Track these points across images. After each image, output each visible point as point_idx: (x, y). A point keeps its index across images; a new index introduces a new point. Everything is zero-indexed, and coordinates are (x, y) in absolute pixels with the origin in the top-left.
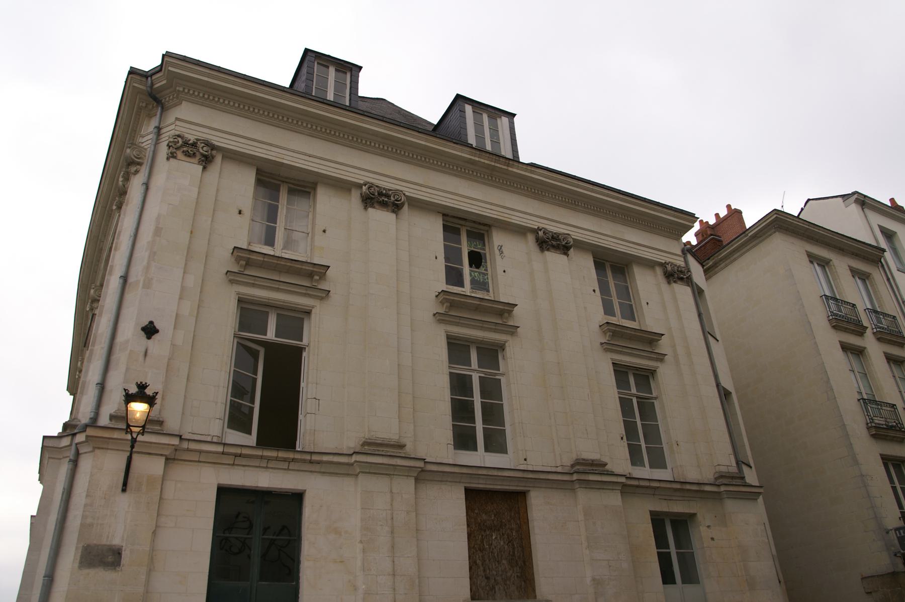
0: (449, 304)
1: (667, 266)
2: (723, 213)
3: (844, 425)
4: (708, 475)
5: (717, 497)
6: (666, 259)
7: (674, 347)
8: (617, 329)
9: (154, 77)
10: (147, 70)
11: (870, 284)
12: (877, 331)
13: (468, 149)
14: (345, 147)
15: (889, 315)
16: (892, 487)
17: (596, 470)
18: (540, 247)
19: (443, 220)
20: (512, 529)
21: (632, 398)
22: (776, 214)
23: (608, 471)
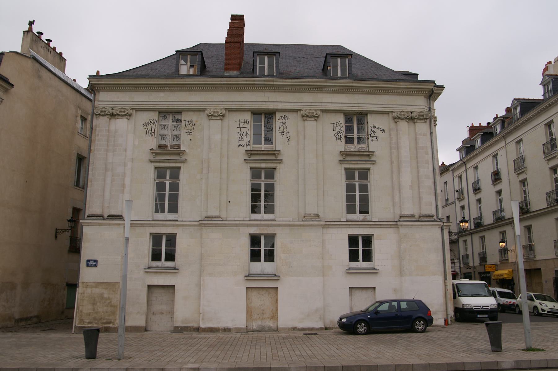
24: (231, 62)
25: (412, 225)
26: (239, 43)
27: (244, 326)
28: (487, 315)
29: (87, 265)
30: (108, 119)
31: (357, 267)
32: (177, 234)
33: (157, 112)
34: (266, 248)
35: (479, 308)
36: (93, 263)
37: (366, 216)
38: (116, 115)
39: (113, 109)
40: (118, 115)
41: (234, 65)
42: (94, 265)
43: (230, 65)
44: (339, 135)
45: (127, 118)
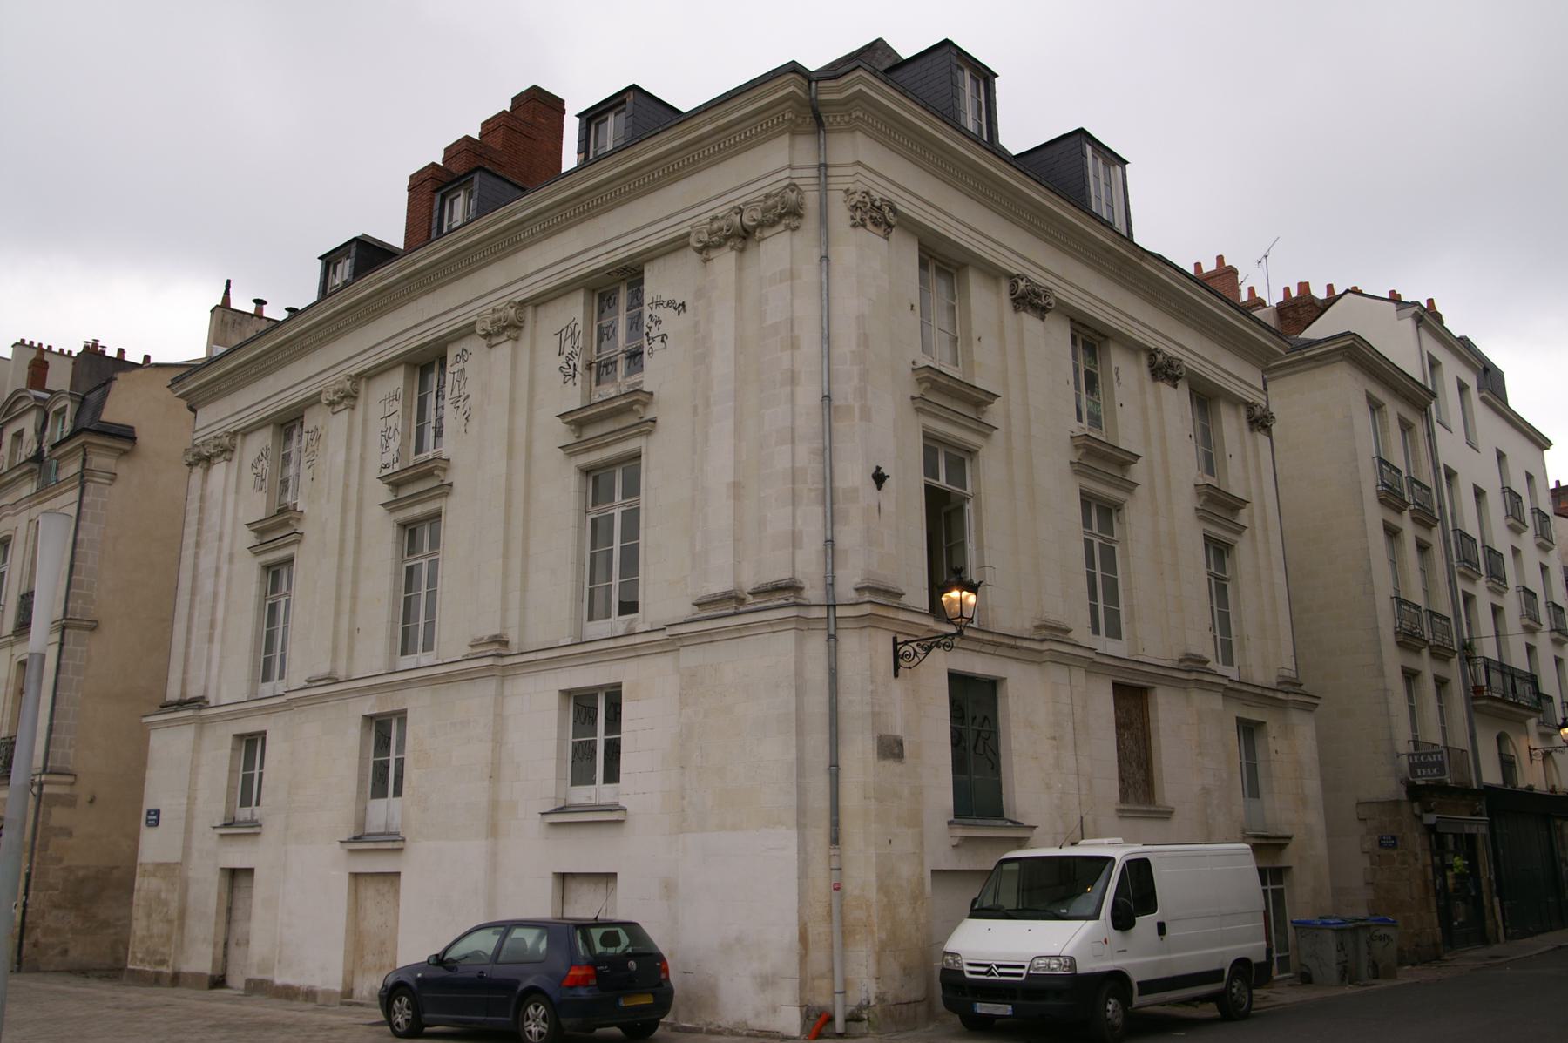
0: (1085, 451)
1: (1020, 281)
2: (1209, 266)
3: (1378, 627)
4: (1272, 681)
5: (1282, 705)
6: (1255, 398)
7: (1008, 417)
8: (950, 384)
9: (821, 84)
10: (811, 70)
11: (1379, 417)
12: (1415, 509)
13: (1111, 233)
14: (945, 184)
15: (1395, 468)
16: (1410, 706)
17: (1057, 636)
18: (1153, 375)
19: (1072, 328)
20: (1137, 729)
21: (1094, 539)
22: (1353, 339)
23: (1209, 669)
25: (708, 632)
27: (339, 988)
28: (1010, 1007)
31: (588, 802)
34: (577, 738)
35: (985, 969)
37: (632, 621)
38: (755, 228)
39: (740, 211)
44: (571, 363)
45: (787, 227)
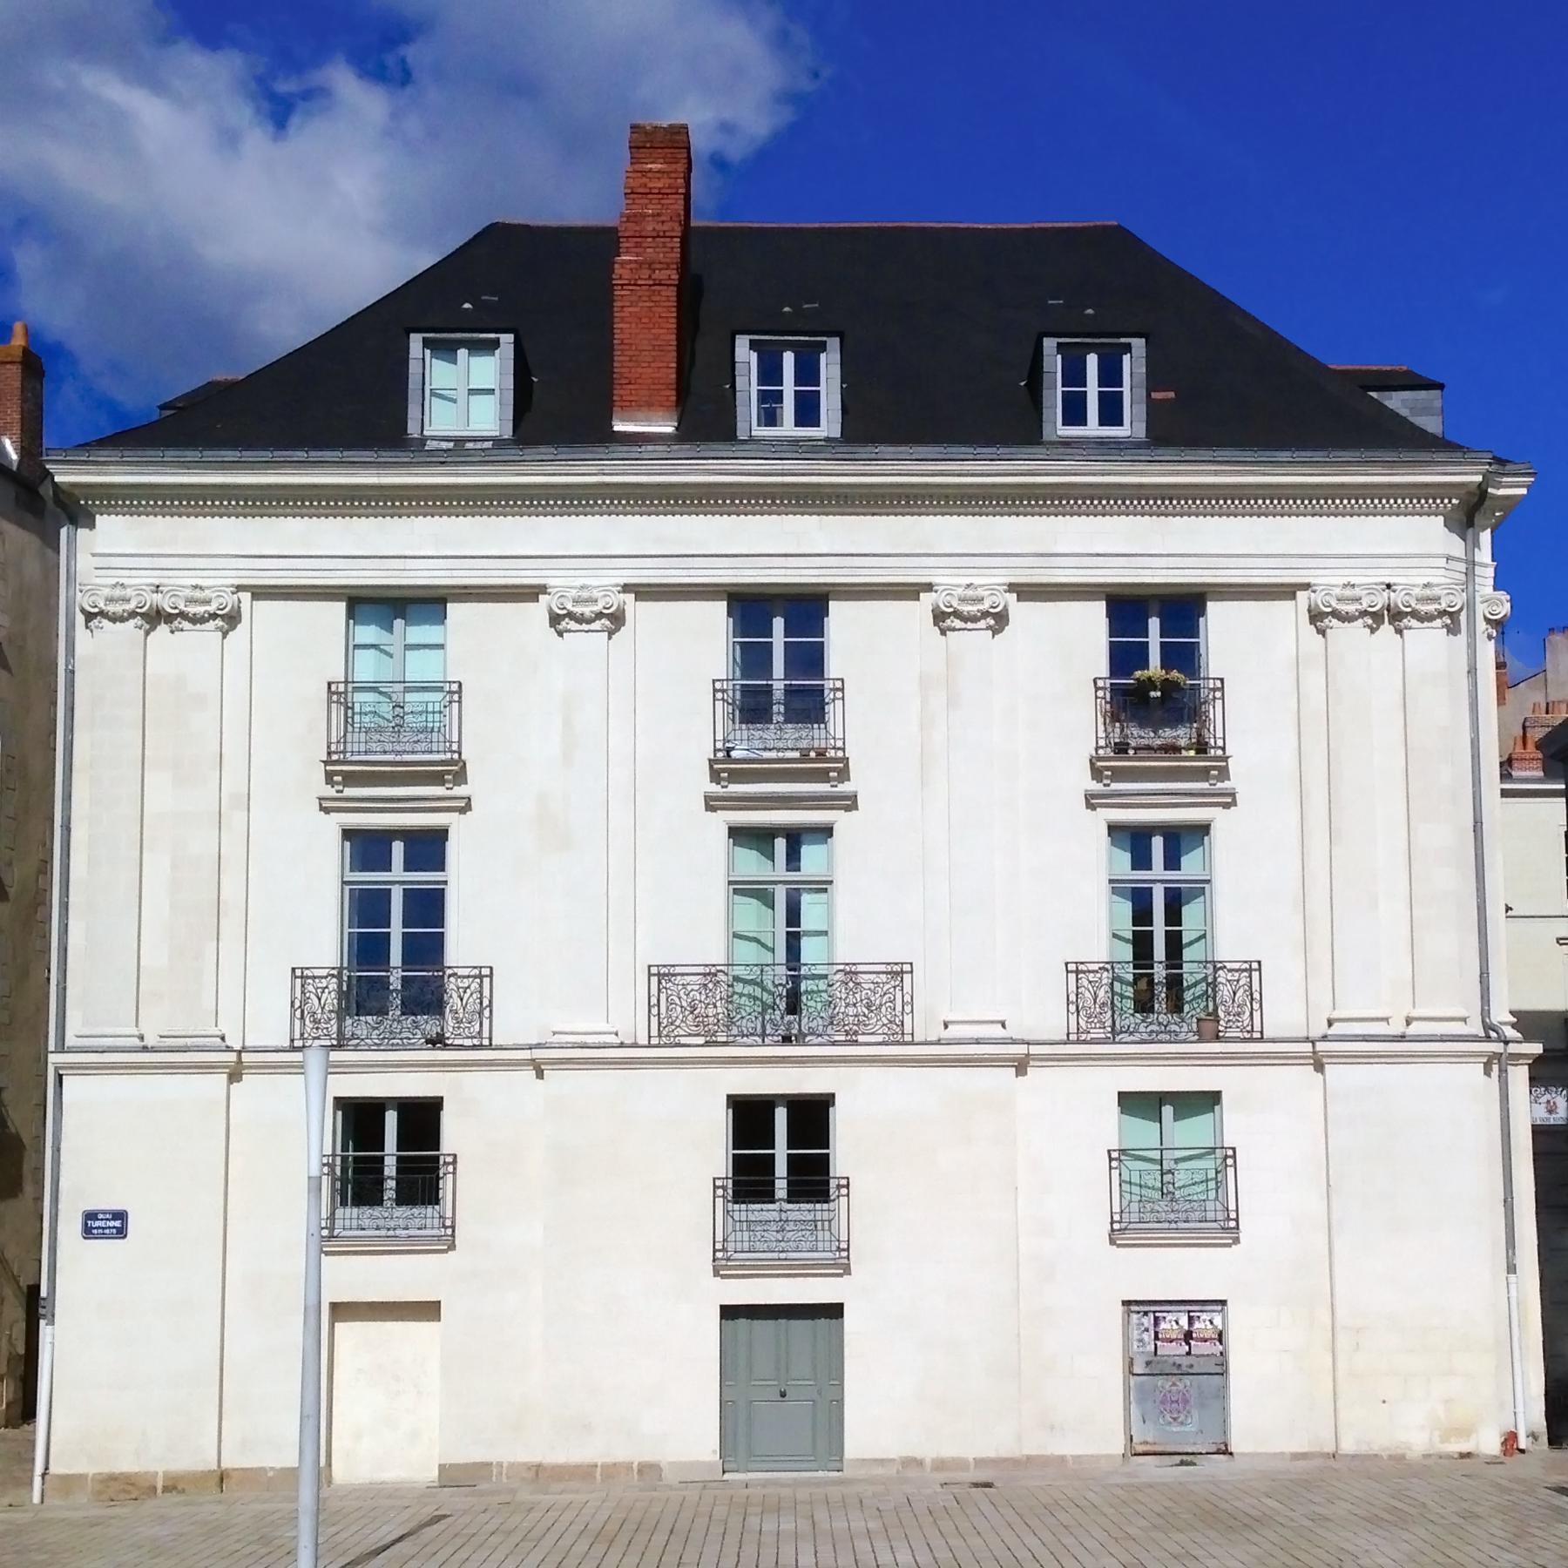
24: (640, 370)
26: (668, 285)
29: (88, 1232)
30: (142, 632)
32: (1175, 1120)
33: (341, 607)
36: (112, 1224)
40: (183, 615)
41: (652, 387)
42: (114, 1231)
43: (636, 387)
